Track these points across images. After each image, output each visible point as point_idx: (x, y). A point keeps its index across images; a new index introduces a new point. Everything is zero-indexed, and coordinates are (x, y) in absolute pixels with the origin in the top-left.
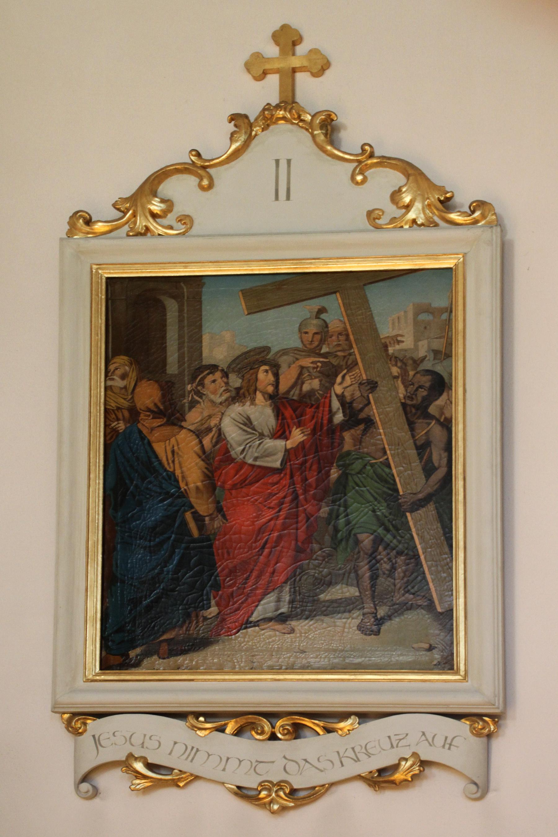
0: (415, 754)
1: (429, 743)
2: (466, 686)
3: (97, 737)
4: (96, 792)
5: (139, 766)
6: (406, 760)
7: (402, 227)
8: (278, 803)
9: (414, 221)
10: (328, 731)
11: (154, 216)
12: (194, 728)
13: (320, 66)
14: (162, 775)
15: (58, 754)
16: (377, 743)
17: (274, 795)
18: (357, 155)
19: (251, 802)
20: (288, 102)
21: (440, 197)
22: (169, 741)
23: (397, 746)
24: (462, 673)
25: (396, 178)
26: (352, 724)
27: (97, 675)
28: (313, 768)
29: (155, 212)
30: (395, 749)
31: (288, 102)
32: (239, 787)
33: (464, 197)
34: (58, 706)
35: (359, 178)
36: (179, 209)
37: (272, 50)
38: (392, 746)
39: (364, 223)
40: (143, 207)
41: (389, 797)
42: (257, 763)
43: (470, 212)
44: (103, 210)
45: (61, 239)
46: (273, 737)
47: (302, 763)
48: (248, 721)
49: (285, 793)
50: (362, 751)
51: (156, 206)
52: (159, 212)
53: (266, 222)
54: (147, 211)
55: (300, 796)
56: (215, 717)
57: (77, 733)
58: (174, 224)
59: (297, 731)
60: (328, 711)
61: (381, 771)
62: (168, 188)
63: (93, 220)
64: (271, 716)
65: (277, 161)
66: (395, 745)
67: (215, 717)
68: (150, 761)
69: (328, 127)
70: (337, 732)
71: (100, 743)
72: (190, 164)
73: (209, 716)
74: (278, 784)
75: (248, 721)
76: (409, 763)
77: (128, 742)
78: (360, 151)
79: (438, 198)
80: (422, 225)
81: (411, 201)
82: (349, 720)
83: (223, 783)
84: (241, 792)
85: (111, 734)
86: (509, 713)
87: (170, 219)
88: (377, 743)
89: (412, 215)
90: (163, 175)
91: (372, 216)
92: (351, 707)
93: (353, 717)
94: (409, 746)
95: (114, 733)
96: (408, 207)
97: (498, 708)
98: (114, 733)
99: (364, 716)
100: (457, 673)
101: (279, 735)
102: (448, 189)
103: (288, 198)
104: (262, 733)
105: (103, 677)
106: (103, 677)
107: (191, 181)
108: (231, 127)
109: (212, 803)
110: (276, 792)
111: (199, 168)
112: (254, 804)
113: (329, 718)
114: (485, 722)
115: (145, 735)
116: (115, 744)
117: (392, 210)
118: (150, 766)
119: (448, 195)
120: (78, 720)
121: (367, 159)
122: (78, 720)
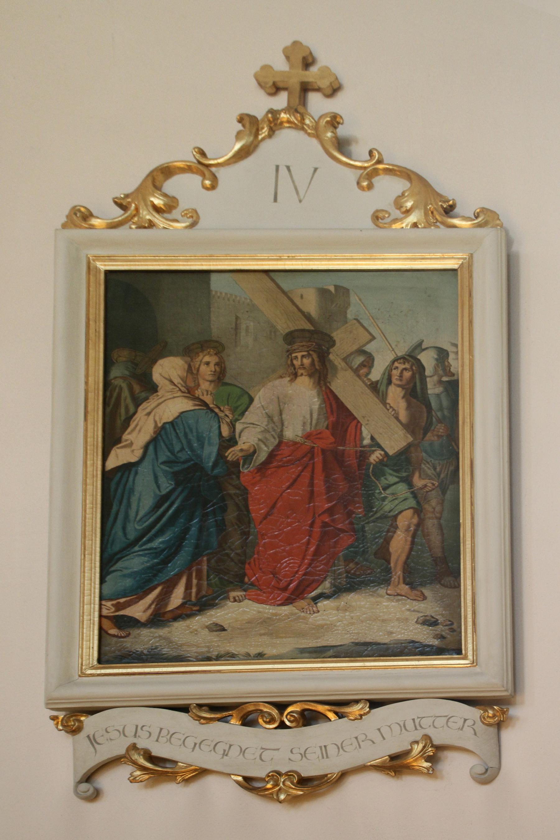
0: (427, 737)
2: (477, 667)
3: (91, 737)
4: (96, 795)
6: (417, 742)
10: (340, 716)
11: (157, 209)
13: (334, 90)
15: (63, 756)
16: (385, 732)
17: (281, 785)
19: (257, 794)
20: (300, 83)
21: (443, 204)
22: (181, 739)
24: (470, 657)
26: (362, 708)
29: (158, 206)
31: (300, 83)
32: (246, 779)
33: (467, 204)
35: (365, 184)
36: (183, 205)
37: (280, 64)
39: (369, 223)
40: (145, 200)
42: (419, 719)
43: (473, 218)
45: (57, 230)
46: (282, 726)
49: (292, 783)
51: (158, 201)
52: (162, 207)
54: (149, 203)
55: (310, 786)
56: (219, 710)
57: (75, 731)
58: (179, 217)
59: (308, 718)
61: (393, 758)
62: (172, 186)
64: (281, 707)
65: (327, 757)
67: (219, 710)
70: (347, 717)
72: (195, 163)
73: (213, 708)
74: (286, 774)
76: (421, 746)
77: (122, 735)
78: (369, 158)
79: (441, 205)
83: (229, 775)
84: (249, 783)
86: (518, 698)
87: (176, 214)
90: (167, 171)
91: (376, 217)
94: (379, 730)
96: (408, 212)
97: (507, 690)
98: (106, 729)
100: (465, 658)
101: (288, 723)
102: (450, 198)
103: (277, 167)
105: (99, 672)
106: (99, 672)
107: (196, 179)
109: (222, 792)
110: (284, 782)
112: (261, 795)
114: (495, 707)
115: (137, 726)
119: (451, 203)
122: (73, 718)
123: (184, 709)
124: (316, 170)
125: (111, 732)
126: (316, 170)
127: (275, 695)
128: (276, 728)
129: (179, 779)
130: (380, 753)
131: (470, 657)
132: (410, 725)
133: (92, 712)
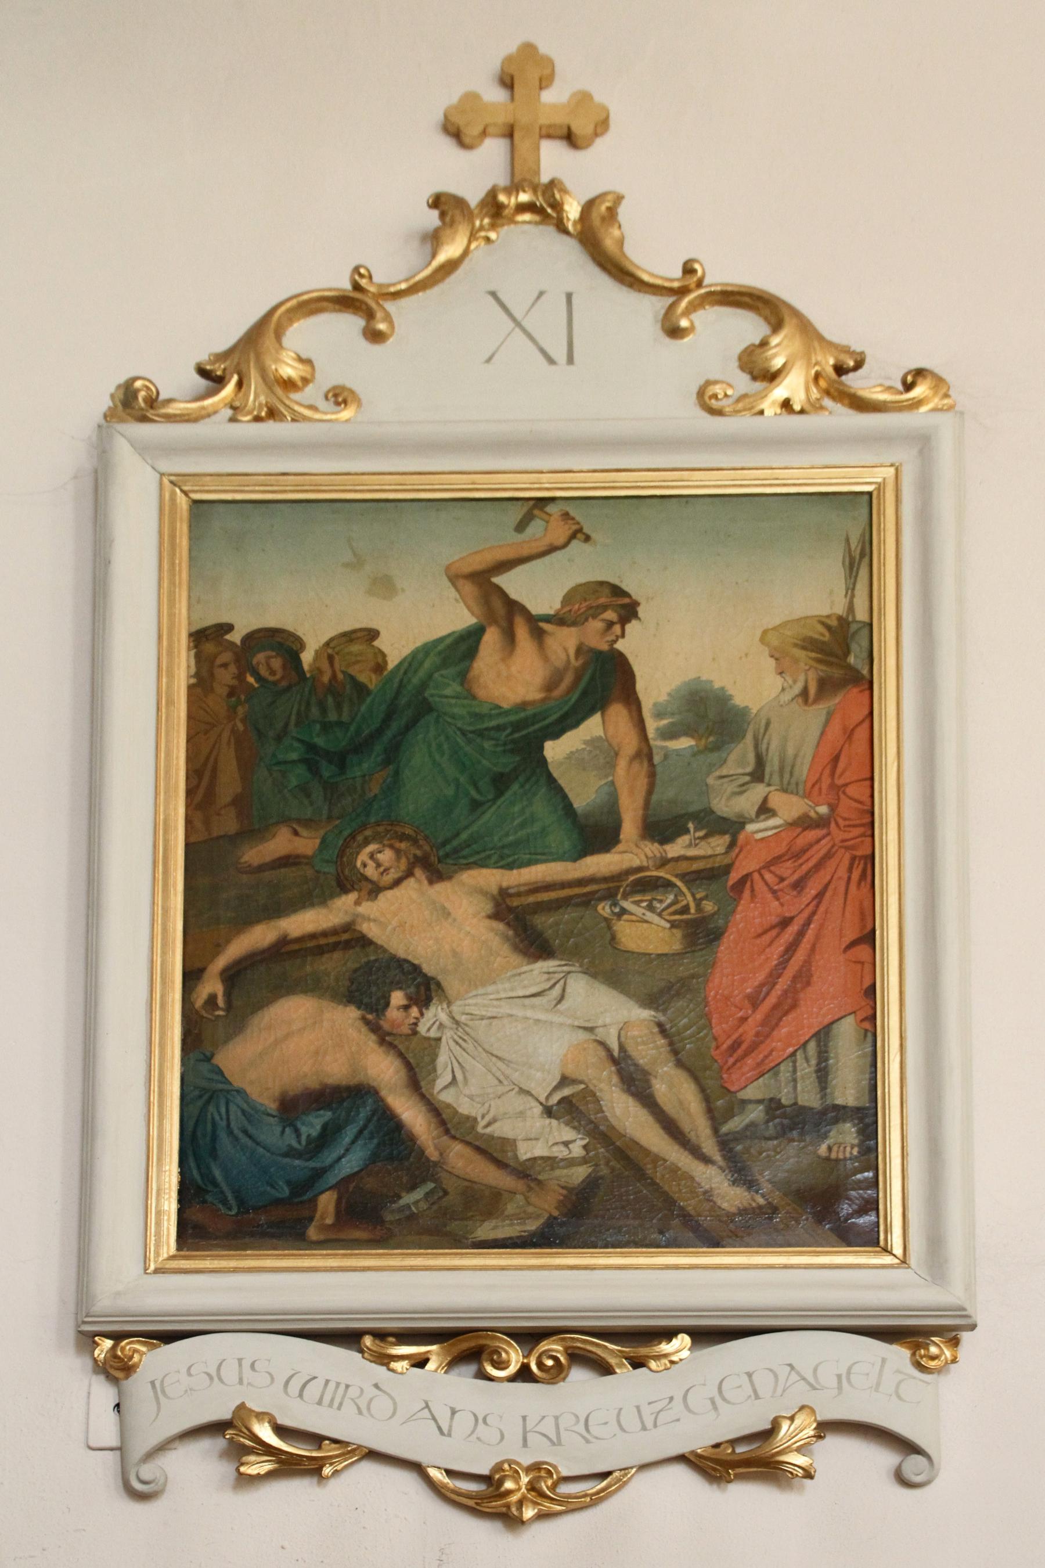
1: (811, 1385)
5: (265, 1433)
7: (762, 412)
8: (536, 1504)
9: (786, 405)
10: (637, 1364)
12: (385, 1360)
14: (305, 1457)
18: (678, 280)
23: (655, 1426)
24: (898, 1250)
25: (747, 327)
27: (173, 1258)
28: (432, 1422)
30: (344, 1381)
31: (523, 169)
34: (90, 1319)
38: (644, 1428)
41: (746, 1496)
43: (900, 387)
44: (176, 381)
46: (524, 1374)
47: (365, 1411)
48: (468, 1346)
50: (575, 1428)
53: (513, 389)
60: (379, 1328)
63: (162, 397)
64: (529, 1337)
66: (649, 1424)
68: (279, 1422)
69: (596, 240)
71: (163, 1392)
75: (468, 1346)
78: (678, 273)
80: (802, 412)
81: (785, 365)
82: (674, 1340)
85: (184, 1370)
88: (699, 1394)
89: (780, 392)
92: (614, 1317)
93: (680, 1336)
95: (189, 1368)
96: (772, 377)
98: (189, 1368)
99: (706, 1336)
104: (500, 1365)
108: (432, 219)
111: (355, 300)
113: (639, 1340)
116: (191, 1389)
117: (743, 383)
118: (281, 1431)
120: (114, 1346)
121: (682, 296)
122: (114, 1346)
123: (347, 1338)
124: (541, 294)
125: (184, 1382)
126: (541, 294)
127: (545, 1314)
128: (512, 1379)
129: (327, 1470)
130: (701, 1434)
131: (898, 1250)
132: (630, 1420)
133: (169, 1337)
